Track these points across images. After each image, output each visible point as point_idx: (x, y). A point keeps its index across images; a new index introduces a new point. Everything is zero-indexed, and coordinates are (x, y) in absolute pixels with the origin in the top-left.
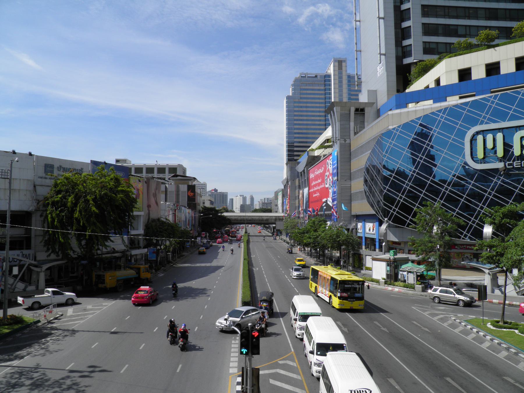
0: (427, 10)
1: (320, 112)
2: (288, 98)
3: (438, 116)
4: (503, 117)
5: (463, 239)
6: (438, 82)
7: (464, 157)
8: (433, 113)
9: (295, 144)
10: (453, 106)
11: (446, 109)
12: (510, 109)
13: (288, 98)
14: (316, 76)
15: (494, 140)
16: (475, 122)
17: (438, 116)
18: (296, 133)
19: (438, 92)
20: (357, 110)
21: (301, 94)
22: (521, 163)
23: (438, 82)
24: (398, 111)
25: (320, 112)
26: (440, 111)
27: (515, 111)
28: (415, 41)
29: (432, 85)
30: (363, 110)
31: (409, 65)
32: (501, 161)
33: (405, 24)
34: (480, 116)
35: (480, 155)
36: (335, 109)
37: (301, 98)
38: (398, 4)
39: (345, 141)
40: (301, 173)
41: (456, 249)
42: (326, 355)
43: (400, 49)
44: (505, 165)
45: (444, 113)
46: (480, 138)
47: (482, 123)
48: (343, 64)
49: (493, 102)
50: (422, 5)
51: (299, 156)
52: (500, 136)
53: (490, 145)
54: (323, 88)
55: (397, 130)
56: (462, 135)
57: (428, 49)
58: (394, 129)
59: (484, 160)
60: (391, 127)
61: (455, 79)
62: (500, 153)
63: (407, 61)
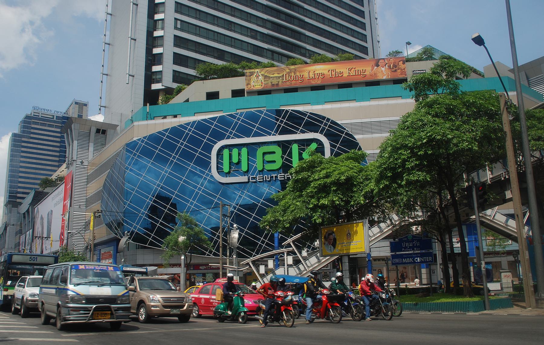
0: (180, 8)
2: (14, 135)
3: (186, 128)
4: (247, 133)
5: (208, 255)
7: (210, 170)
8: (181, 126)
11: (194, 122)
12: (254, 127)
13: (14, 135)
15: (239, 154)
16: (221, 137)
17: (186, 128)
18: (21, 177)
20: (98, 131)
22: (263, 177)
24: (145, 122)
26: (188, 124)
27: (258, 128)
28: (166, 69)
30: (104, 132)
31: (158, 91)
33: (156, 51)
34: (227, 131)
35: (226, 169)
36: (73, 126)
38: (151, 30)
40: (24, 214)
41: (201, 269)
42: (34, 108)
43: (152, 21)
44: (249, 179)
46: (226, 152)
47: (228, 138)
49: (239, 119)
50: (175, 36)
51: (23, 198)
52: (244, 151)
53: (235, 160)
55: (143, 141)
56: (209, 149)
57: (178, 77)
58: (139, 140)
59: (228, 174)
60: (135, 139)
62: (244, 168)
63: (155, 86)
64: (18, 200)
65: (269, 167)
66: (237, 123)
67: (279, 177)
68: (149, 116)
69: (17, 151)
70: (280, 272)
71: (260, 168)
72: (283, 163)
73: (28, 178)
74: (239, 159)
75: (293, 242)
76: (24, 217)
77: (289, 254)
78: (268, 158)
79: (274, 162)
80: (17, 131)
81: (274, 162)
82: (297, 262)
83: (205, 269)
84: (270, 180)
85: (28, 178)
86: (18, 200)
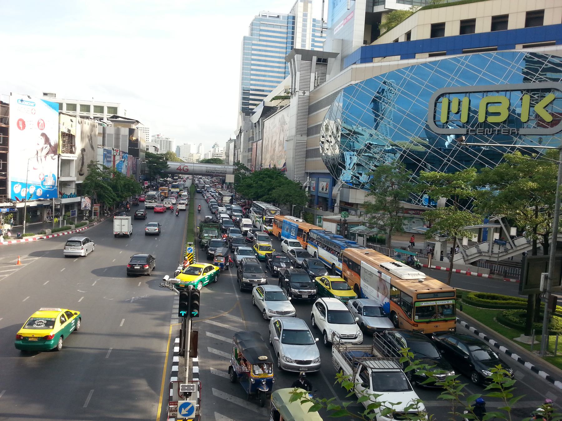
1: (280, 57)
2: (245, 38)
6: (408, 35)
8: (399, 70)
9: (251, 92)
10: (421, 64)
12: (480, 72)
14: (278, 17)
19: (407, 48)
20: (319, 60)
21: (260, 35)
23: (408, 35)
24: (364, 65)
25: (280, 57)
26: (406, 69)
29: (402, 39)
30: (325, 61)
31: (380, 14)
32: (463, 127)
37: (260, 40)
39: (304, 93)
44: (468, 131)
45: (410, 71)
48: (309, 5)
54: (285, 30)
58: (356, 84)
61: (427, 35)
62: (464, 119)
63: (378, 9)
64: (251, 107)
65: (491, 119)
66: (460, 68)
67: (502, 131)
68: (329, 203)
69: (247, 59)
70: (484, 247)
71: (481, 119)
72: (509, 115)
73: (259, 80)
74: (459, 109)
75: (502, 219)
76: (256, 126)
77: (496, 230)
78: (491, 109)
79: (498, 114)
80: (247, 34)
81: (498, 114)
82: (502, 242)
83: (414, 214)
84: (492, 134)
85: (259, 80)
86: (251, 107)
